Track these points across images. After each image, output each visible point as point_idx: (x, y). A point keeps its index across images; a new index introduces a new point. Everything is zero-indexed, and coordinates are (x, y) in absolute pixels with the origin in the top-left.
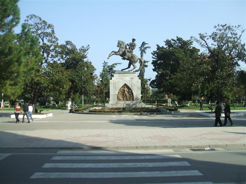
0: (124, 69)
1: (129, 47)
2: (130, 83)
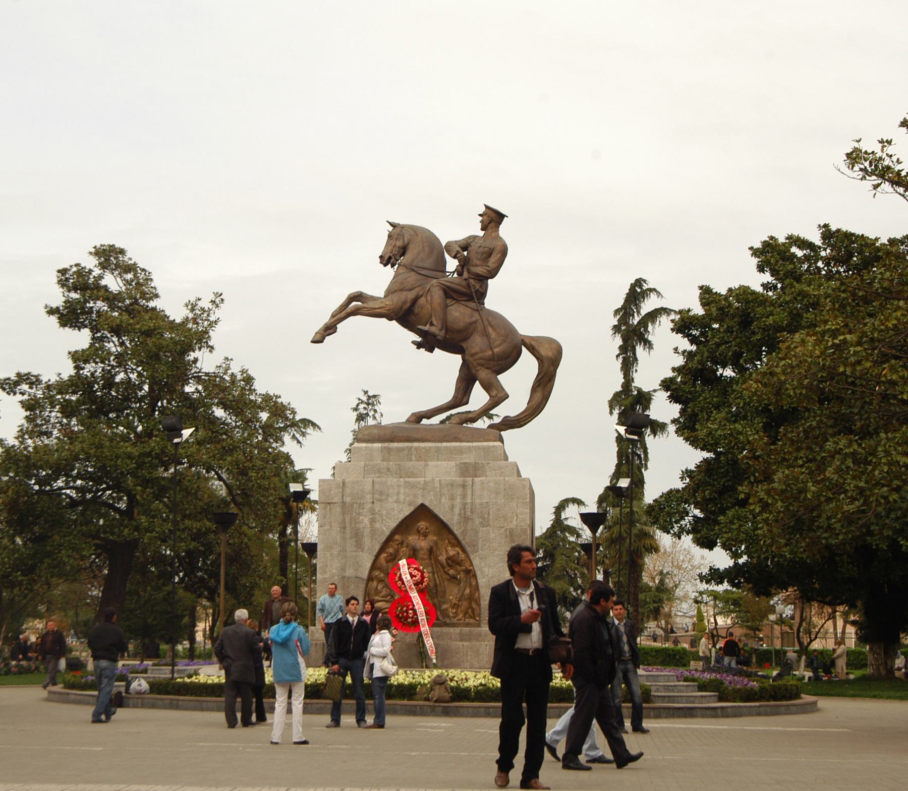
0: (429, 414)
2: (452, 498)
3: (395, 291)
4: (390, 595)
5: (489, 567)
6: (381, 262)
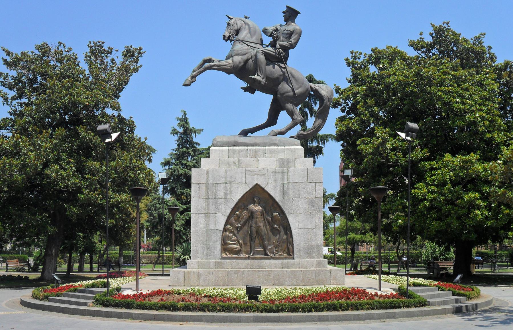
1: (271, 39)
3: (194, 77)
6: (224, 39)
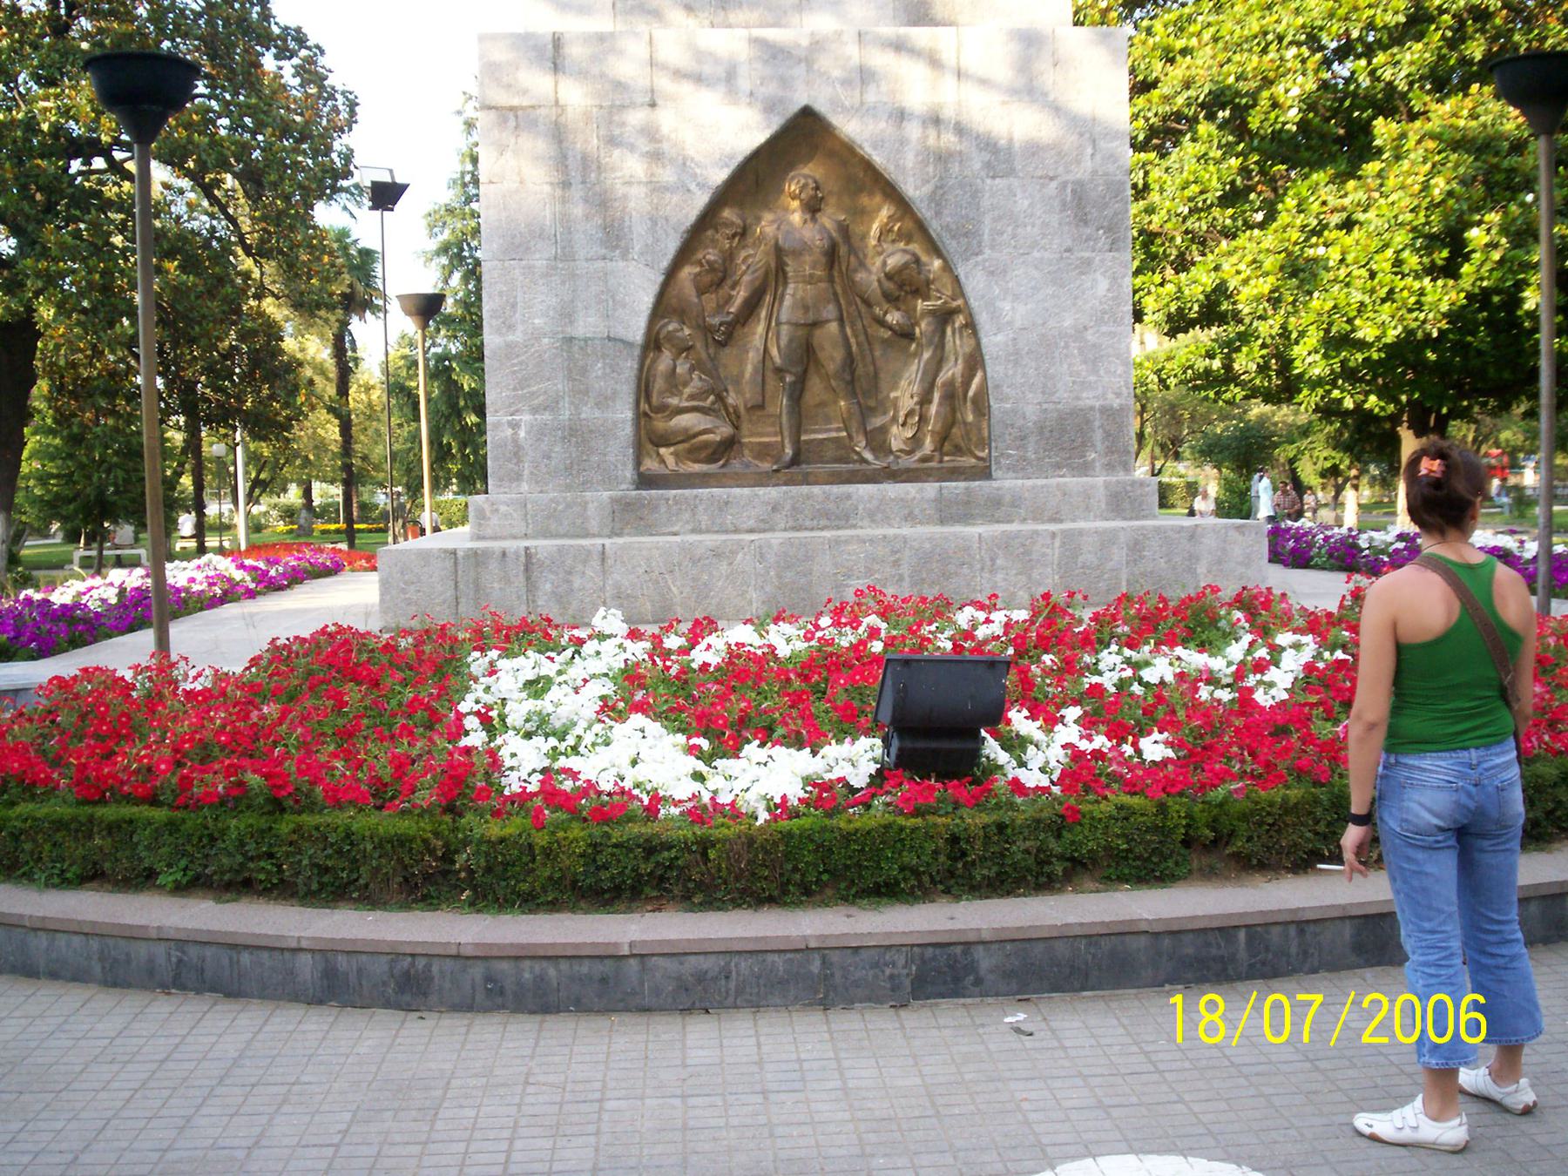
4: (712, 391)
5: (1016, 297)
